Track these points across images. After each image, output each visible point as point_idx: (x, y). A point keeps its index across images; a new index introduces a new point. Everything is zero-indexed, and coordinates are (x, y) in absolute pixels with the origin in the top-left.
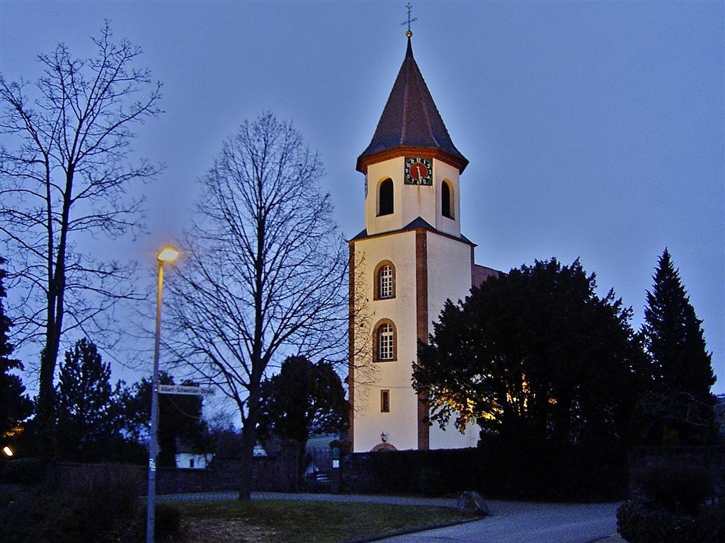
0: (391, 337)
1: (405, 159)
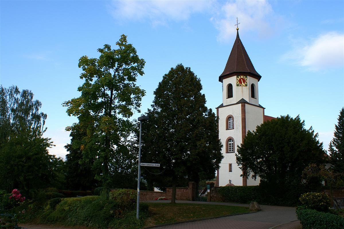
0: (232, 144)
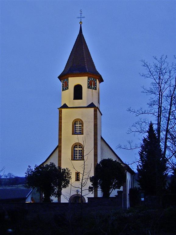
1: (88, 78)
